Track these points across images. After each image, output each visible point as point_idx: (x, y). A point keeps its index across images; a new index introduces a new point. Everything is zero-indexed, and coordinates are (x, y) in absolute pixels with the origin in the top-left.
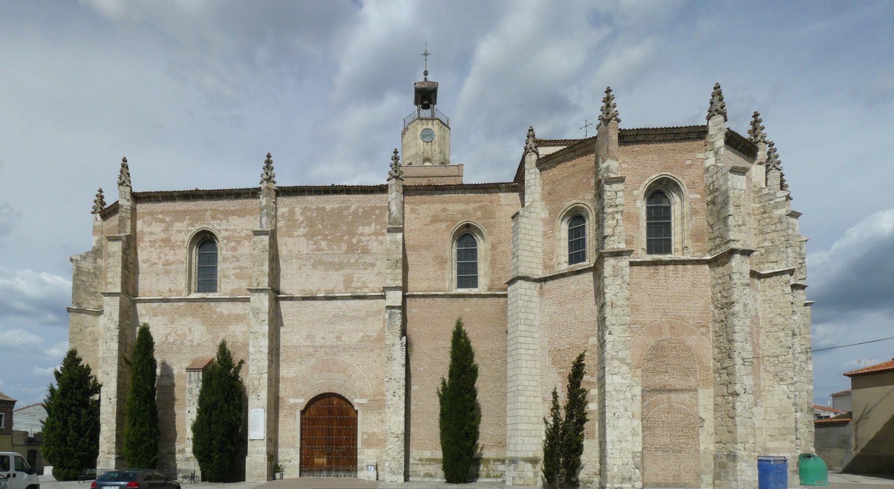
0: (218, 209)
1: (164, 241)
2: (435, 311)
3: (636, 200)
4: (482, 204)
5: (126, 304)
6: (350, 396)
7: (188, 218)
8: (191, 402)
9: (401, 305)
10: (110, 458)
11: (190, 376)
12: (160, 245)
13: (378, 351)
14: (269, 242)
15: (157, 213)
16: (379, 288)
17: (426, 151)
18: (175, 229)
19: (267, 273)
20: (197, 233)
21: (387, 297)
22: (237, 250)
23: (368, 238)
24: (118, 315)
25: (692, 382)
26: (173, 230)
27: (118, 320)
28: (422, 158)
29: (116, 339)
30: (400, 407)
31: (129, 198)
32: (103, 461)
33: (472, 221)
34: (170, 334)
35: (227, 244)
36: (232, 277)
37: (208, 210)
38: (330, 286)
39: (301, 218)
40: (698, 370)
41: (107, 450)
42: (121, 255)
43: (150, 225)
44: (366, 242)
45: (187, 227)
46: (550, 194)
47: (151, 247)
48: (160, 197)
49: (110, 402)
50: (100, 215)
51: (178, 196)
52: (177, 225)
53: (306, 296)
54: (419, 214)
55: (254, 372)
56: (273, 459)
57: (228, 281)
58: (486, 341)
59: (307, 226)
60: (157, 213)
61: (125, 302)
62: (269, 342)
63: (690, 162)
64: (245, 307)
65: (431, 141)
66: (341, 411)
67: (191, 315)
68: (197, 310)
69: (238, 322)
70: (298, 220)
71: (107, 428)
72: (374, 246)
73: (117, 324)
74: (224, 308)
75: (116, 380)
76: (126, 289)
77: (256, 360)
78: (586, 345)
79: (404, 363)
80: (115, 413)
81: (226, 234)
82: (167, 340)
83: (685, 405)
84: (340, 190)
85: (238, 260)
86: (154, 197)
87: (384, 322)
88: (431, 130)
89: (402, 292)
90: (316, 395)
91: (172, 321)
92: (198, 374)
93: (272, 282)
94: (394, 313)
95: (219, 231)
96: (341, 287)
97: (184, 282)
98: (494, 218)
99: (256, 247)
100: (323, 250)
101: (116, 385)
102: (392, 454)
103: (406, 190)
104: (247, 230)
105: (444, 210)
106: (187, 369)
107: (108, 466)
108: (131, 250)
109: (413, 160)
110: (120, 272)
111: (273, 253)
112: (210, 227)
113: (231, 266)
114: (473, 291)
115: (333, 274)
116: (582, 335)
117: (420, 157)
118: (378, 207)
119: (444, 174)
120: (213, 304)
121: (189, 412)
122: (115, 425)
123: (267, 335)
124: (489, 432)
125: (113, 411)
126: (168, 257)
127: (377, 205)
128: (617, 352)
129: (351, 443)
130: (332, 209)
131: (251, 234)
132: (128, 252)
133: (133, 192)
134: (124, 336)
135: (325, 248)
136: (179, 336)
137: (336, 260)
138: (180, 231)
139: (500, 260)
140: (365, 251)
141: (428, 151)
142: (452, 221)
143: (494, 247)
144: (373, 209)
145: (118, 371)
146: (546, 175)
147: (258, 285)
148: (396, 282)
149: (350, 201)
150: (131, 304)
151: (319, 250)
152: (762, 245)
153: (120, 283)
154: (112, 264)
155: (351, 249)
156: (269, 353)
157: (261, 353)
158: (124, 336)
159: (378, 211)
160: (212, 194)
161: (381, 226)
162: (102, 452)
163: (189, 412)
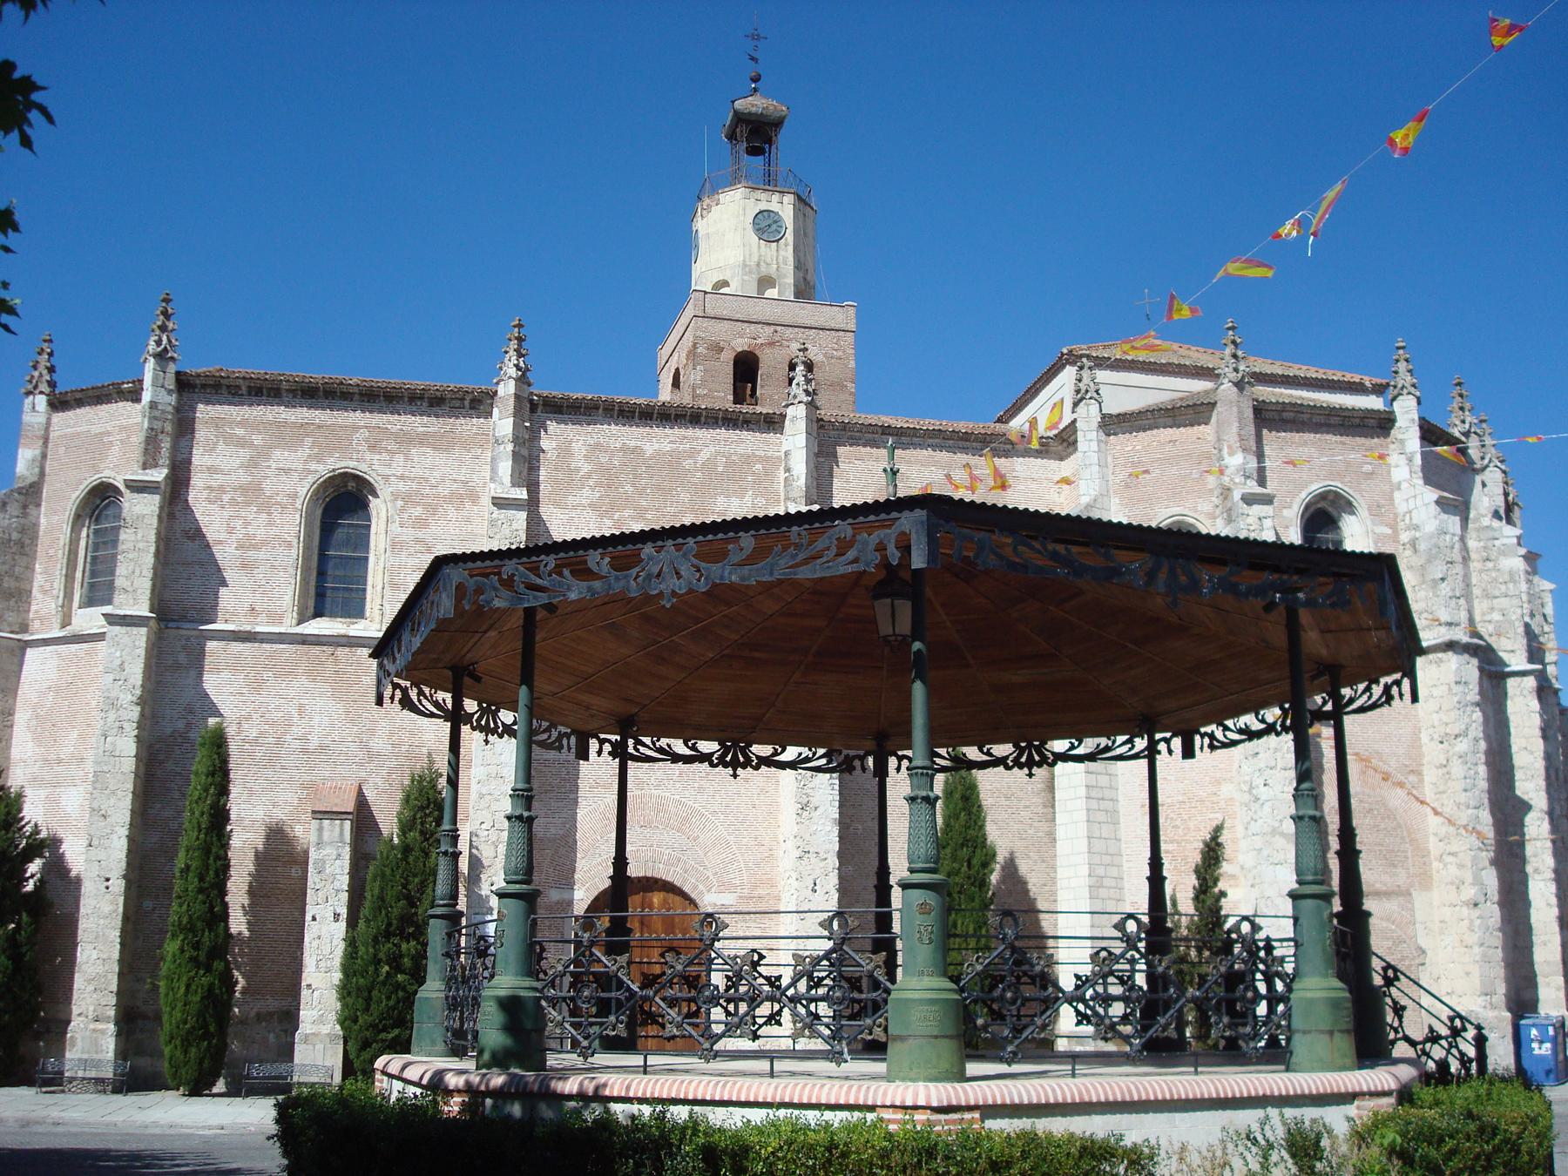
0: (387, 428)
1: (243, 489)
3: (1287, 527)
6: (696, 887)
7: (308, 441)
8: (320, 893)
10: (103, 1032)
11: (320, 829)
12: (233, 499)
15: (231, 423)
18: (274, 465)
22: (426, 526)
24: (141, 671)
25: (1401, 878)
26: (269, 467)
28: (755, 277)
29: (131, 730)
31: (172, 387)
32: (83, 1038)
34: (248, 718)
35: (402, 510)
39: (586, 468)
40: (1409, 854)
41: (94, 1011)
43: (213, 449)
46: (1127, 486)
48: (244, 388)
49: (107, 888)
51: (293, 392)
52: (280, 457)
54: (848, 481)
55: (483, 826)
60: (231, 423)
63: (1370, 467)
67: (309, 673)
68: (321, 663)
70: (578, 470)
73: (138, 692)
75: (127, 833)
77: (489, 797)
78: (1215, 799)
83: (1393, 923)
86: (228, 387)
91: (257, 686)
92: (342, 825)
95: (386, 478)
101: (126, 847)
107: (97, 1053)
112: (364, 467)
116: (1207, 778)
117: (750, 272)
119: (809, 322)
121: (314, 919)
122: (118, 947)
125: (115, 911)
126: (251, 530)
127: (757, 453)
128: (1281, 821)
130: (658, 453)
136: (273, 724)
141: (769, 261)
144: (748, 460)
146: (1118, 448)
152: (1488, 618)
154: (130, 545)
157: (502, 780)
159: (758, 466)
162: (80, 1015)
163: (314, 919)
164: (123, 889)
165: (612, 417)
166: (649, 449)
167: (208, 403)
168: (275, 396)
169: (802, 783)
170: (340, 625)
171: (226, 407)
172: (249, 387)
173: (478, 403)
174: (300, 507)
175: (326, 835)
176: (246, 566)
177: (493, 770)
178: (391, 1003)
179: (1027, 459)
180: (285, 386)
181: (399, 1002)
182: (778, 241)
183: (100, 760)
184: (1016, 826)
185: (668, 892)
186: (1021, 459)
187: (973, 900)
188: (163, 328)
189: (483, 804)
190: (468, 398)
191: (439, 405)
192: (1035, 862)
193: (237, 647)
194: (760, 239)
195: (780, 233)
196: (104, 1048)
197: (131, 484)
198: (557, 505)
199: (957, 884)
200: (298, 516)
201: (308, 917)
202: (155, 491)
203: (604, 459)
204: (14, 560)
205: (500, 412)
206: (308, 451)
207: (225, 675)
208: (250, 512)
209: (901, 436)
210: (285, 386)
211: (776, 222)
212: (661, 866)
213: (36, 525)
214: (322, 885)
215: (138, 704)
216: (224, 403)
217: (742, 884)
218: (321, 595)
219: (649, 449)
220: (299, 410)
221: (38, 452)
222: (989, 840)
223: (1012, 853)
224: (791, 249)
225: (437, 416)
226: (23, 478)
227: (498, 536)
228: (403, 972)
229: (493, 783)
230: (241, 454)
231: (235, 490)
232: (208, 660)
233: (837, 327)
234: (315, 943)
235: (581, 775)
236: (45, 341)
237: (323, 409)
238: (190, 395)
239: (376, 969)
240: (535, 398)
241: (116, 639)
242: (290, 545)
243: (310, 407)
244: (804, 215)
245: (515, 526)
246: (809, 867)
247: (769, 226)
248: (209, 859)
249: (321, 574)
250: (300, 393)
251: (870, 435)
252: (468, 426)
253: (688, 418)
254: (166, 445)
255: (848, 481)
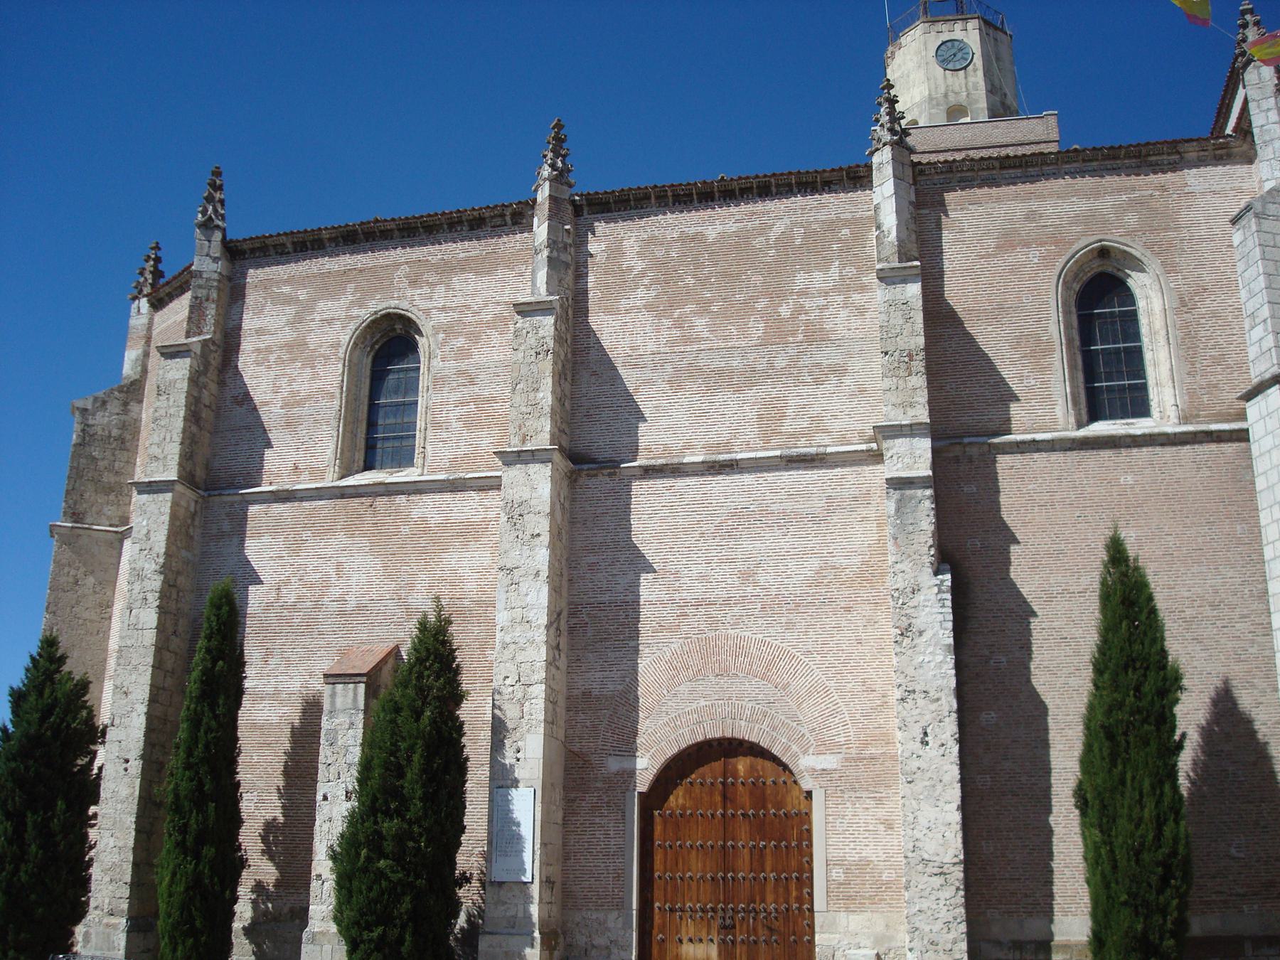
0: (427, 260)
1: (289, 347)
2: (1030, 487)
4: (1137, 194)
5: (187, 509)
6: (788, 748)
8: (332, 768)
9: (930, 473)
10: (115, 926)
11: (333, 695)
13: (866, 610)
14: (556, 329)
16: (861, 433)
17: (953, 91)
18: (318, 318)
19: (547, 409)
20: (373, 322)
21: (887, 455)
23: (822, 302)
24: (164, 538)
26: (313, 320)
27: (163, 550)
28: (943, 108)
30: (946, 778)
32: (97, 934)
33: (1114, 238)
34: (287, 582)
35: (445, 342)
36: (454, 425)
37: (400, 265)
38: (720, 433)
39: (639, 265)
42: (185, 389)
43: (261, 311)
44: (817, 312)
45: (348, 309)
47: (258, 364)
49: (126, 770)
50: (149, 301)
52: (326, 307)
53: (653, 462)
55: (508, 682)
56: (557, 943)
57: (445, 435)
58: (1195, 569)
59: (655, 282)
61: (183, 503)
62: (550, 595)
64: (486, 502)
65: (965, 68)
66: (759, 794)
68: (360, 516)
69: (465, 545)
70: (630, 269)
71: (112, 842)
72: (840, 321)
73: (161, 560)
74: (428, 508)
76: (191, 471)
77: (513, 646)
79: (951, 641)
80: (136, 801)
81: (443, 318)
82: (278, 597)
84: (741, 189)
85: (472, 383)
86: (275, 246)
87: (879, 525)
88: (962, 41)
89: (930, 439)
90: (684, 746)
91: (296, 547)
92: (355, 690)
93: (560, 431)
94: (911, 498)
95: (427, 312)
96: (751, 433)
97: (332, 446)
98: (1177, 229)
99: (520, 344)
100: (699, 340)
101: (144, 725)
102: (927, 929)
103: (922, 172)
104: (498, 303)
105: (1030, 216)
106: (326, 676)
107: (109, 950)
108: (209, 375)
109: (921, 113)
110: (180, 430)
111: (566, 354)
112: (405, 305)
113: (454, 397)
114: (1140, 426)
115: (727, 403)
118: (847, 220)
120: (401, 499)
121: (325, 798)
122: (134, 833)
123: (545, 573)
124: (1233, 851)
126: (295, 386)
129: (794, 894)
130: (722, 236)
131: (509, 312)
132: (202, 379)
133: (228, 239)
134: (174, 591)
135: (706, 334)
137: (735, 363)
138: (330, 322)
139: (1209, 338)
140: (817, 336)
141: (957, 89)
142: (1056, 243)
143: (1184, 304)
144: (832, 226)
145: (152, 686)
147: (524, 442)
148: (911, 412)
149: (768, 213)
150: (198, 509)
151: (687, 340)
153: (177, 457)
155: (777, 333)
156: (548, 627)
157: (528, 625)
158: (174, 591)
159: (845, 231)
160: (413, 225)
161: (858, 268)
162: (96, 908)
163: (325, 798)
164: (139, 771)
165: (666, 205)
166: (712, 233)
167: (258, 266)
168: (319, 248)
169: (901, 601)
170: (385, 475)
171: (274, 268)
172: (293, 243)
173: (518, 218)
174: (343, 356)
175: (339, 701)
176: (291, 424)
177: (518, 613)
178: (373, 895)
179: (1202, 169)
180: (325, 235)
181: (383, 894)
182: (965, 68)
183: (124, 634)
184: (1230, 645)
185: (756, 756)
186: (1194, 171)
187: (1148, 744)
188: (210, 199)
189: (507, 654)
190: (508, 212)
191: (479, 227)
192: (1264, 692)
193: (278, 508)
194: (945, 70)
195: (966, 60)
196: (116, 944)
197: (165, 351)
198: (608, 311)
199: (1122, 721)
200: (340, 366)
201: (319, 797)
202: (186, 354)
203: (659, 252)
204: (114, 455)
205: (539, 219)
206: (350, 298)
207: (266, 539)
208: (294, 369)
209: (1027, 166)
210: (325, 235)
211: (961, 50)
212: (743, 723)
213: (137, 421)
214: (334, 759)
215: (161, 573)
216: (273, 264)
217: (848, 742)
218: (370, 447)
219: (712, 233)
220: (342, 258)
221: (140, 351)
222: (1170, 658)
223: (1226, 682)
224: (980, 73)
225: (478, 239)
226: (128, 376)
227: (522, 348)
228: (386, 857)
229: (518, 629)
230: (288, 311)
231: (281, 348)
232: (250, 525)
233: (1037, 139)
234: (326, 827)
235: (642, 617)
236: (152, 249)
237: (365, 252)
238: (242, 262)
239: (356, 851)
240: (577, 198)
241: (144, 508)
242: (332, 396)
243: (352, 253)
244: (996, 40)
245: (541, 333)
246: (915, 712)
247: (955, 55)
248: (199, 731)
249: (372, 425)
250: (340, 239)
251: (985, 173)
252: (511, 243)
253: (755, 191)
254: (211, 311)
255: (962, 231)
